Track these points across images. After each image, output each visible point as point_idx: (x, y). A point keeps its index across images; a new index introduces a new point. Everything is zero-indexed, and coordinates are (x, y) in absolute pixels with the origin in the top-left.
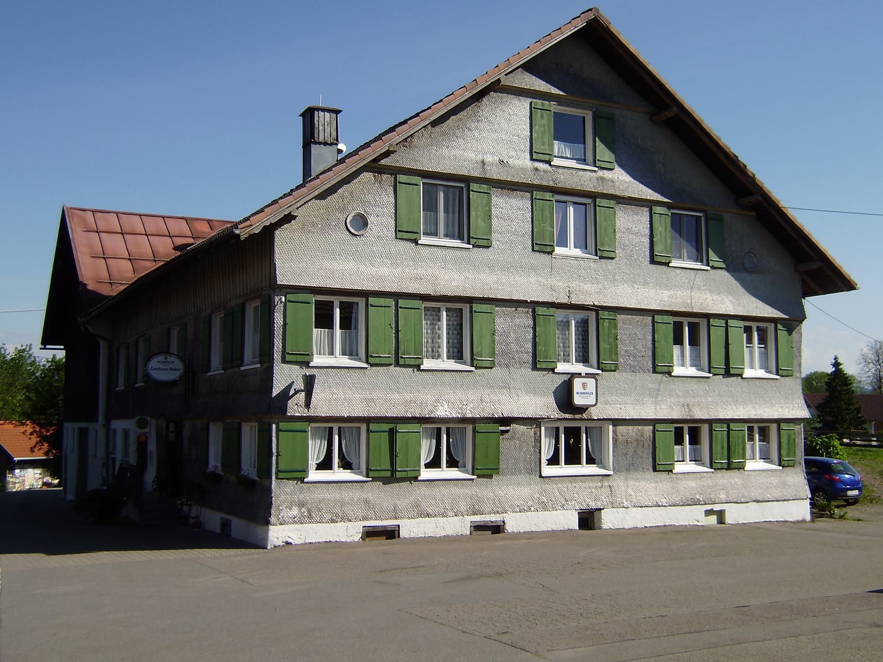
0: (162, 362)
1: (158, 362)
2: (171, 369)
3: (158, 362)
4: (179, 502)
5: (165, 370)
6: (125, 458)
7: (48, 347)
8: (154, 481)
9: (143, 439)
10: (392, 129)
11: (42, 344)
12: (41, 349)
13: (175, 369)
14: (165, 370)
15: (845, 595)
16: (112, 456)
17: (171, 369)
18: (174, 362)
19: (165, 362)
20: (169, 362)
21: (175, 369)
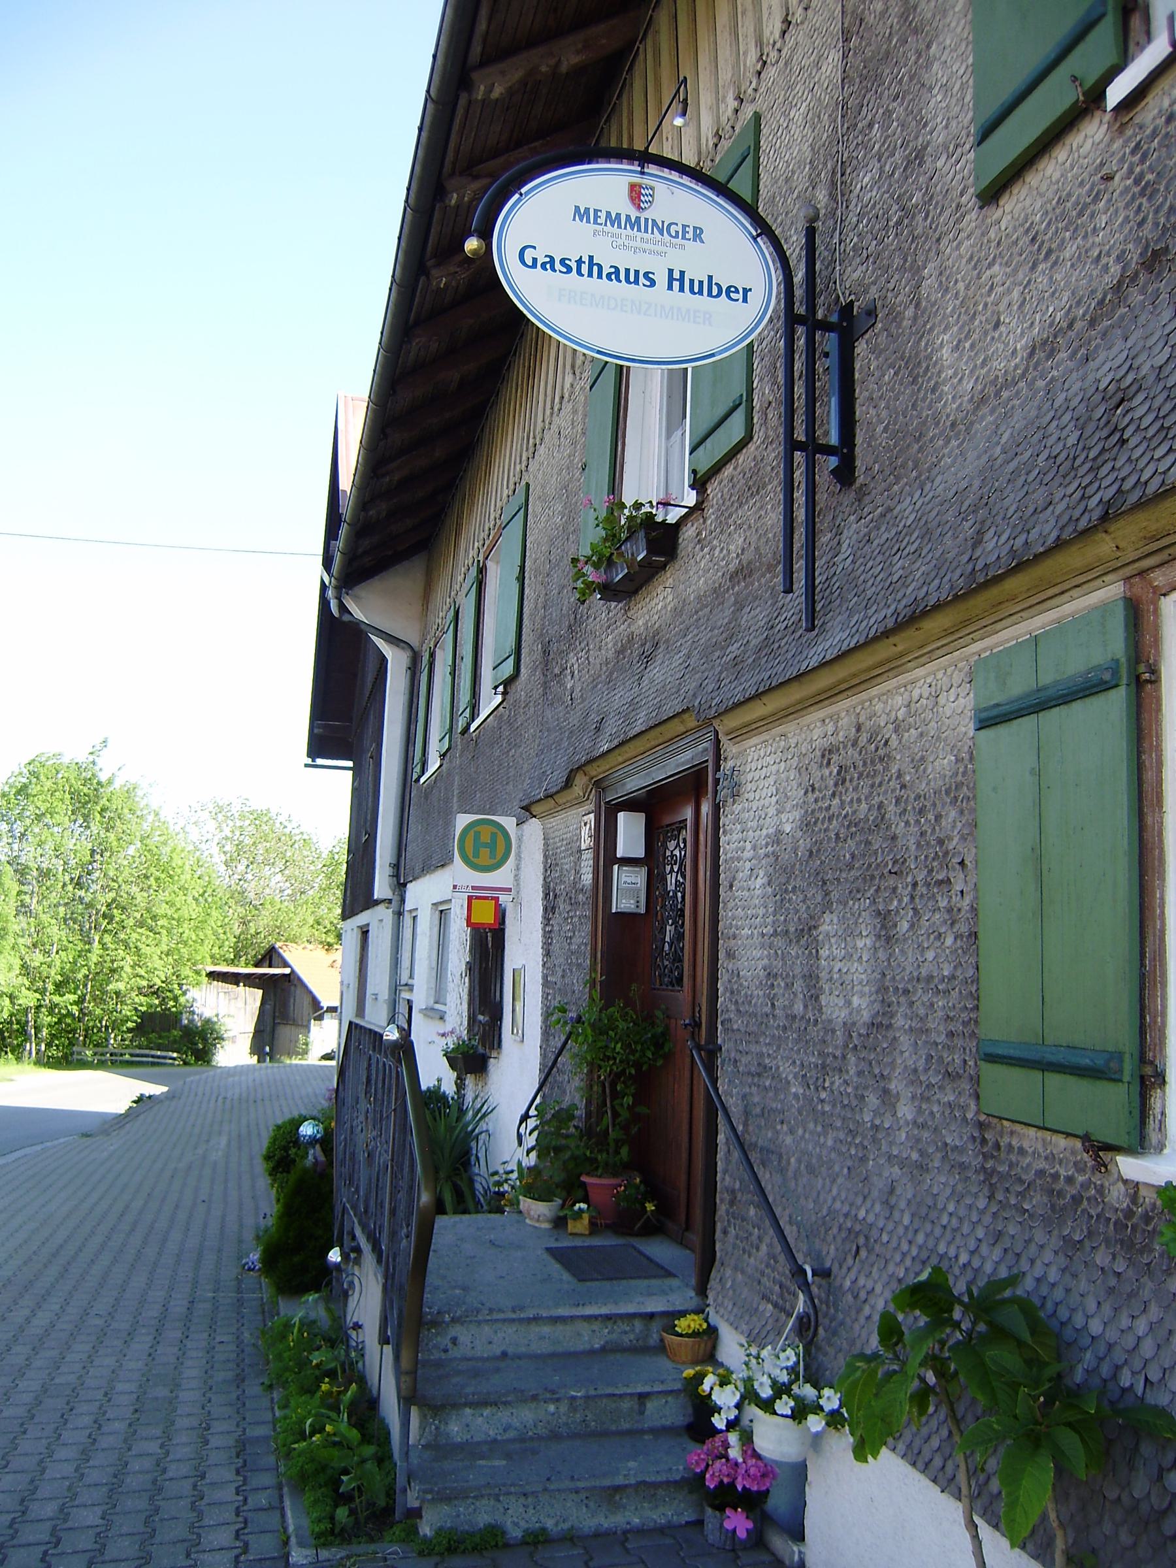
0: (614, 219)
1: (581, 214)
2: (676, 280)
3: (581, 214)
4: (992, 1464)
5: (633, 278)
6: (436, 1003)
7: (319, 761)
8: (525, 1117)
9: (485, 915)
10: (1030, 607)
11: (309, 755)
12: (306, 766)
13: (710, 288)
14: (633, 278)
15: (736, 1328)
16: (405, 995)
17: (676, 280)
18: (698, 234)
19: (635, 224)
20: (661, 228)
21: (710, 288)
